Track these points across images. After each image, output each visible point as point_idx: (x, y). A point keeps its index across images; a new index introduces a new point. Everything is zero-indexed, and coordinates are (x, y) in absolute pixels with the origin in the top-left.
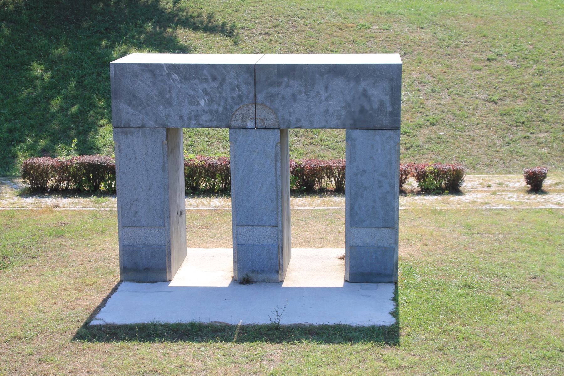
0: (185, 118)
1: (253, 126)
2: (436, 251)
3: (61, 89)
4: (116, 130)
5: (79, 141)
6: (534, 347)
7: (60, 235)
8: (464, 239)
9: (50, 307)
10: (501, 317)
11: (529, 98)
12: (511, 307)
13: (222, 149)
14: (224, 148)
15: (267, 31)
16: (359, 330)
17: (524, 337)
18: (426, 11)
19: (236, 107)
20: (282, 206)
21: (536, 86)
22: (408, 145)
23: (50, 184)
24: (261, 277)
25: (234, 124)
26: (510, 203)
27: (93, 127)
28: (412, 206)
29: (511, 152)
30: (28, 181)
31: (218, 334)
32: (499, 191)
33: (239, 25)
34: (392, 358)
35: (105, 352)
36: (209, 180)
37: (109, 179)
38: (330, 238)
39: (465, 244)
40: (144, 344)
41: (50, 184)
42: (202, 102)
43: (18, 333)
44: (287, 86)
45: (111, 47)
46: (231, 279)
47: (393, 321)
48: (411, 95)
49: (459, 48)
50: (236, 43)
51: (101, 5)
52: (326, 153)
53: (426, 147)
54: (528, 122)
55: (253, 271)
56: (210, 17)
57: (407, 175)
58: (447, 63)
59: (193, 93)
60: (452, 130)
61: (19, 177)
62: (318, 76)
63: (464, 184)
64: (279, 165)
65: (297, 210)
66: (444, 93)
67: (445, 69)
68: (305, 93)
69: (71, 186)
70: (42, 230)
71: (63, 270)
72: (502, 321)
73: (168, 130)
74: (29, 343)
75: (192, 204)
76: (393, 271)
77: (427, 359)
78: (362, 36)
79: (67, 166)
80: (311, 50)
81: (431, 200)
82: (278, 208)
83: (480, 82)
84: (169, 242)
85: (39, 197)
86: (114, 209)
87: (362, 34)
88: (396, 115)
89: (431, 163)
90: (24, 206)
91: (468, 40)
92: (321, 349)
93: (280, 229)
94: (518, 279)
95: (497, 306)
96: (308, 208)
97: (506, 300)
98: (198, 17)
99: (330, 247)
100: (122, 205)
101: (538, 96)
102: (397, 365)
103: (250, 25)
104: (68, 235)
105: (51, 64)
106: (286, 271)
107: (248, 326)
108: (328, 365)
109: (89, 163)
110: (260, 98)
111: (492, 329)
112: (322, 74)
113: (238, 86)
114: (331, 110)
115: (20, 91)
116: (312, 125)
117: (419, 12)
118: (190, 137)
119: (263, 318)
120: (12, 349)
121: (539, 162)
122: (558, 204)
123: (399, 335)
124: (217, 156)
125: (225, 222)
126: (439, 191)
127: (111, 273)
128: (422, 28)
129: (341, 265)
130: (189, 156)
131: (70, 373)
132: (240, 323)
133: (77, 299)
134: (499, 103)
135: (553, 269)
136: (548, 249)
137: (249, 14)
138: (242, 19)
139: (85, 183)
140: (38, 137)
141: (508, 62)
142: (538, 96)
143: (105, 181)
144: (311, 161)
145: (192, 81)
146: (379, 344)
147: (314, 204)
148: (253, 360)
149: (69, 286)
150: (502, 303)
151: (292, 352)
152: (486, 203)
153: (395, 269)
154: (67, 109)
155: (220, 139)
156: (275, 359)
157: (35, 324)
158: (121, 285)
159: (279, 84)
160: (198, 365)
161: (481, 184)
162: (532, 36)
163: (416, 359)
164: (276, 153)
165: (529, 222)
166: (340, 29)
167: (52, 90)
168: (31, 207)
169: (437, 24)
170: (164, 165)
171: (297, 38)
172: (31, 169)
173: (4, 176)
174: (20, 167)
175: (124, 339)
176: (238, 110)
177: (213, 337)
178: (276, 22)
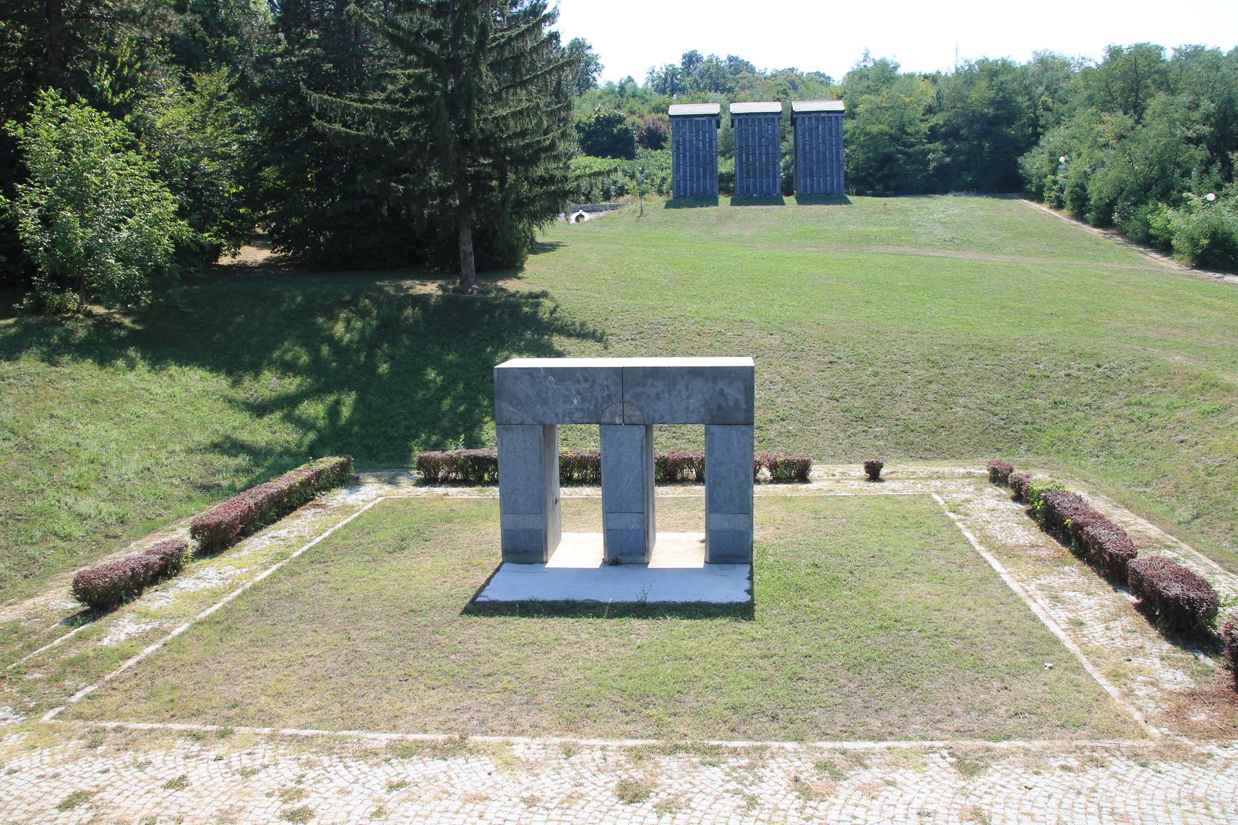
7: (449, 520)
8: (812, 523)
17: (865, 610)
23: (440, 475)
24: (628, 559)
25: (604, 420)
27: (479, 423)
38: (692, 523)
41: (440, 475)
42: (575, 401)
43: (414, 607)
44: (652, 386)
45: (495, 353)
50: (606, 348)
55: (622, 554)
56: (582, 325)
66: (792, 392)
73: (544, 426)
75: (565, 492)
81: (782, 487)
84: (546, 526)
88: (750, 411)
89: (781, 454)
92: (683, 625)
101: (874, 395)
103: (618, 332)
107: (617, 603)
110: (627, 397)
111: (837, 604)
112: (683, 376)
114: (691, 408)
115: (417, 393)
116: (674, 421)
119: (631, 597)
121: (876, 453)
126: (789, 480)
130: (563, 449)
135: (890, 548)
136: (885, 531)
140: (431, 433)
142: (874, 395)
159: (644, 385)
160: (572, 638)
163: (769, 632)
168: (424, 495)
171: (660, 343)
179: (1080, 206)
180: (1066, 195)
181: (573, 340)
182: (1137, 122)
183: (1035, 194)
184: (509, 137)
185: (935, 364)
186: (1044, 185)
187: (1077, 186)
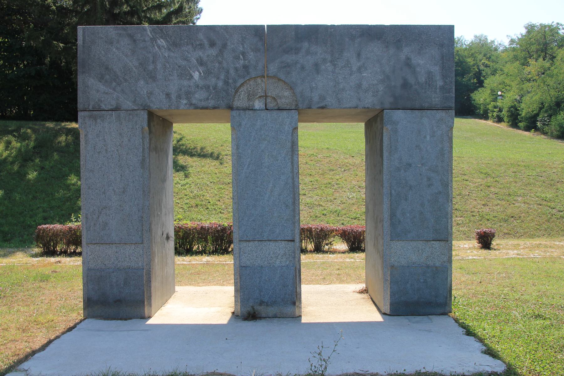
0: (173, 97)
1: (263, 107)
19: (241, 81)
24: (271, 310)
25: (237, 104)
33: (223, 153)
42: (196, 75)
44: (308, 52)
50: (221, 164)
56: (202, 149)
59: (184, 63)
62: (347, 40)
76: (447, 298)
113: (243, 54)
114: (365, 85)
145: (184, 48)
159: (297, 51)
170: (144, 160)
176: (242, 85)
179: (514, 119)
180: (504, 113)
181: (195, 159)
182: (552, 65)
183: (483, 115)
184: (148, 9)
185: (487, 175)
186: (488, 109)
187: (512, 107)
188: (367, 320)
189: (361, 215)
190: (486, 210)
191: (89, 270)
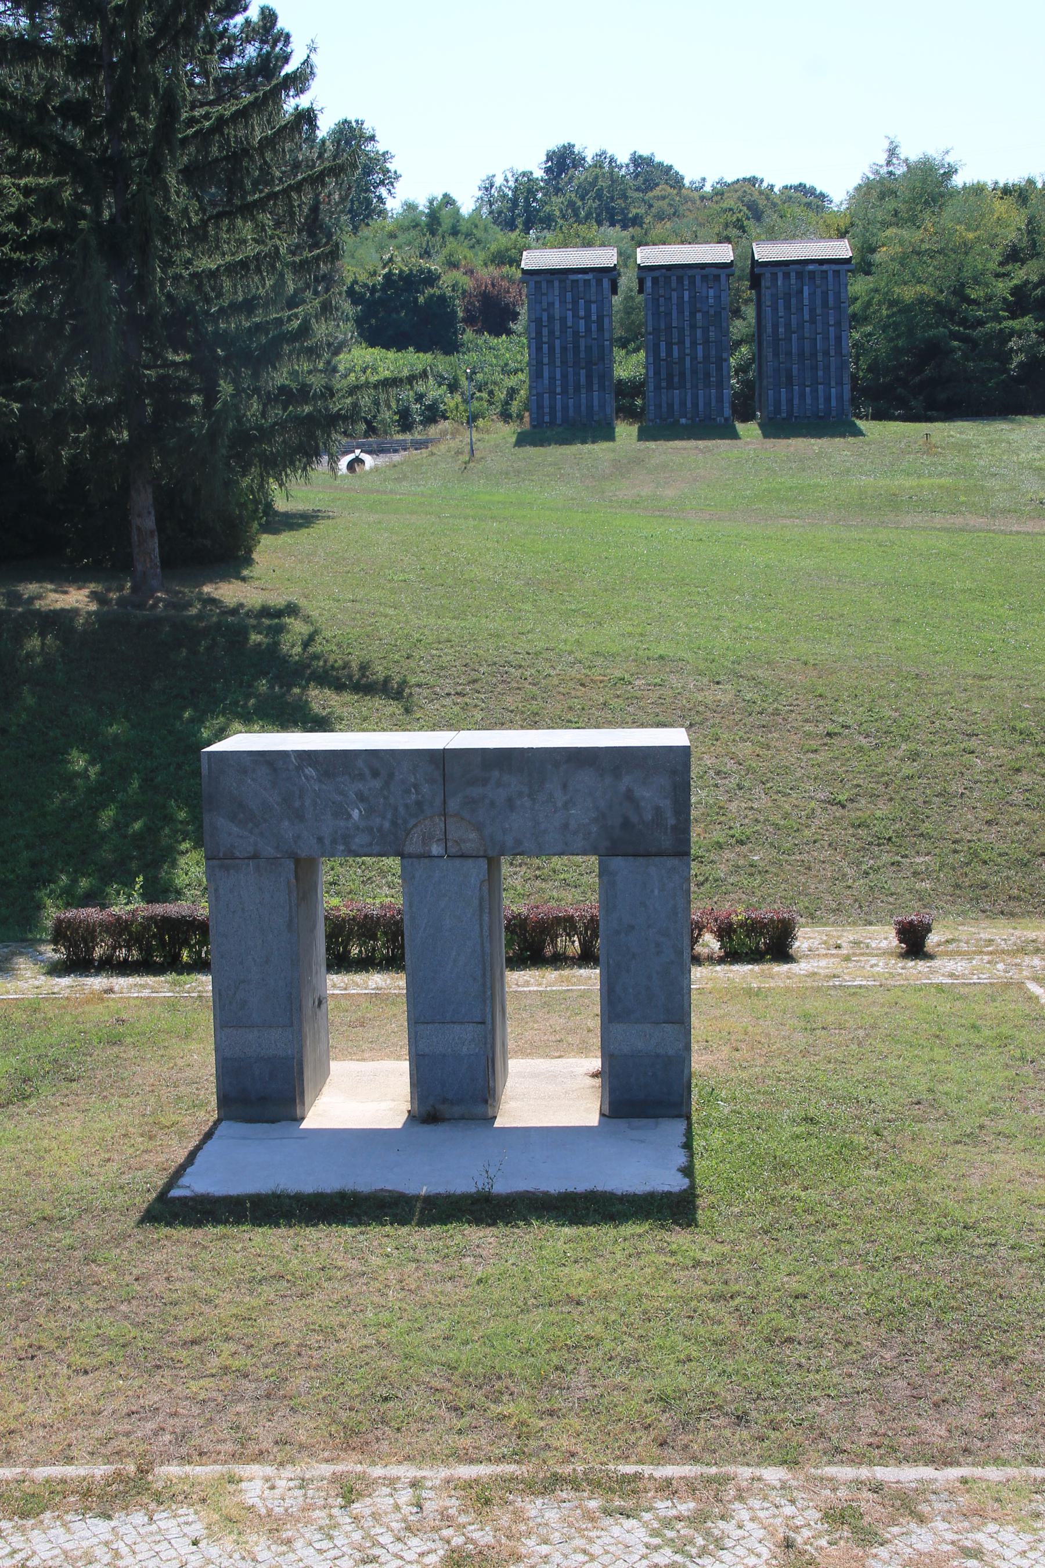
0: (327, 842)
1: (442, 851)
2: (753, 1060)
3: (117, 792)
4: (211, 862)
5: (146, 879)
6: (921, 1223)
7: (115, 1041)
8: (801, 1039)
9: (100, 1166)
10: (867, 1172)
11: (898, 797)
12: (882, 1154)
13: (385, 888)
14: (389, 887)
15: (459, 689)
16: (628, 1201)
17: (906, 1205)
18: (724, 656)
19: (413, 822)
20: (492, 988)
21: (908, 777)
22: (701, 878)
23: (98, 952)
24: (457, 1110)
25: (409, 849)
26: (873, 976)
27: (169, 855)
28: (714, 984)
29: (871, 888)
30: (63, 950)
31: (386, 1210)
32: (854, 954)
33: (413, 680)
34: (684, 1248)
35: (195, 1245)
36: (365, 943)
37: (196, 943)
39: (801, 1048)
40: (260, 1230)
41: (98, 952)
42: (355, 814)
43: (49, 1210)
45: (199, 720)
46: (407, 1115)
47: (685, 1183)
48: (703, 794)
49: (779, 714)
50: (407, 711)
51: (184, 652)
52: (563, 894)
53: (731, 881)
54: (897, 837)
55: (444, 1101)
56: (364, 667)
57: (700, 930)
58: (762, 740)
59: (339, 798)
60: (774, 852)
61: (47, 941)
62: (550, 767)
63: (797, 944)
64: (486, 918)
65: (516, 992)
66: (758, 790)
67: (758, 750)
68: (529, 796)
69: (133, 956)
70: (85, 1032)
71: (122, 1101)
72: (869, 1180)
73: (297, 861)
74: (68, 1228)
75: (337, 984)
76: (682, 1096)
77: (744, 1249)
78: (618, 697)
79: (126, 921)
80: (534, 723)
82: (485, 992)
83: (816, 770)
85: (81, 975)
86: (204, 994)
87: (618, 693)
89: (740, 908)
90: (55, 991)
91: (795, 703)
92: (561, 1237)
93: (490, 1027)
94: (892, 1106)
95: (859, 1154)
96: (535, 988)
97: (873, 1142)
98: (344, 668)
99: (574, 1057)
100: (220, 990)
102: (694, 1259)
103: (431, 680)
104: (129, 1040)
105: (98, 751)
106: (499, 1100)
107: (438, 1196)
108: (576, 1262)
109: (163, 916)
110: (453, 805)
113: (415, 786)
116: (541, 851)
117: (712, 657)
118: (332, 869)
120: (40, 1239)
122: (951, 975)
123: (695, 1208)
124: (378, 901)
125: (394, 1015)
126: (755, 957)
127: (203, 1105)
128: (718, 683)
129: (593, 1087)
130: (331, 902)
131: (136, 1280)
132: (424, 1191)
133: (146, 1151)
134: (849, 805)
136: (939, 1053)
137: (429, 662)
138: (418, 670)
139: (157, 950)
141: (861, 738)
143: (191, 947)
144: (537, 907)
145: (339, 779)
146: (662, 1224)
147: (545, 981)
148: (447, 1256)
149: (130, 1129)
150: (866, 1148)
151: (515, 1241)
152: (834, 976)
153: (685, 1094)
154: (127, 826)
155: (382, 871)
156: (484, 1253)
157: (76, 1196)
158: (220, 1128)
159: (485, 782)
160: (354, 1265)
161: (825, 943)
162: (896, 696)
163: (726, 1249)
164: (481, 900)
165: (906, 1008)
166: (583, 685)
167: (101, 794)
168: (66, 993)
169: (741, 676)
170: (291, 921)
171: (510, 701)
172: (67, 928)
173: (23, 940)
174: (49, 924)
175: (225, 1222)
176: (415, 826)
177: (378, 1217)
178: (474, 675)
181: (348, 697)
184: (222, 310)
188: (577, 1125)
189: (708, 851)
190: (991, 835)
191: (225, 1059)
